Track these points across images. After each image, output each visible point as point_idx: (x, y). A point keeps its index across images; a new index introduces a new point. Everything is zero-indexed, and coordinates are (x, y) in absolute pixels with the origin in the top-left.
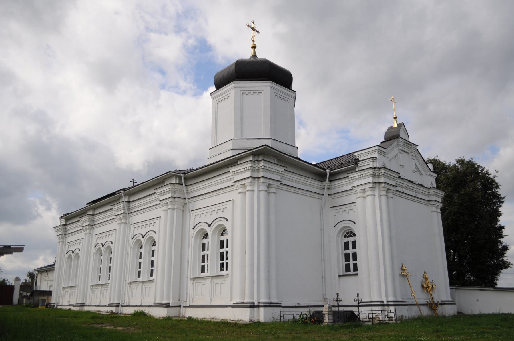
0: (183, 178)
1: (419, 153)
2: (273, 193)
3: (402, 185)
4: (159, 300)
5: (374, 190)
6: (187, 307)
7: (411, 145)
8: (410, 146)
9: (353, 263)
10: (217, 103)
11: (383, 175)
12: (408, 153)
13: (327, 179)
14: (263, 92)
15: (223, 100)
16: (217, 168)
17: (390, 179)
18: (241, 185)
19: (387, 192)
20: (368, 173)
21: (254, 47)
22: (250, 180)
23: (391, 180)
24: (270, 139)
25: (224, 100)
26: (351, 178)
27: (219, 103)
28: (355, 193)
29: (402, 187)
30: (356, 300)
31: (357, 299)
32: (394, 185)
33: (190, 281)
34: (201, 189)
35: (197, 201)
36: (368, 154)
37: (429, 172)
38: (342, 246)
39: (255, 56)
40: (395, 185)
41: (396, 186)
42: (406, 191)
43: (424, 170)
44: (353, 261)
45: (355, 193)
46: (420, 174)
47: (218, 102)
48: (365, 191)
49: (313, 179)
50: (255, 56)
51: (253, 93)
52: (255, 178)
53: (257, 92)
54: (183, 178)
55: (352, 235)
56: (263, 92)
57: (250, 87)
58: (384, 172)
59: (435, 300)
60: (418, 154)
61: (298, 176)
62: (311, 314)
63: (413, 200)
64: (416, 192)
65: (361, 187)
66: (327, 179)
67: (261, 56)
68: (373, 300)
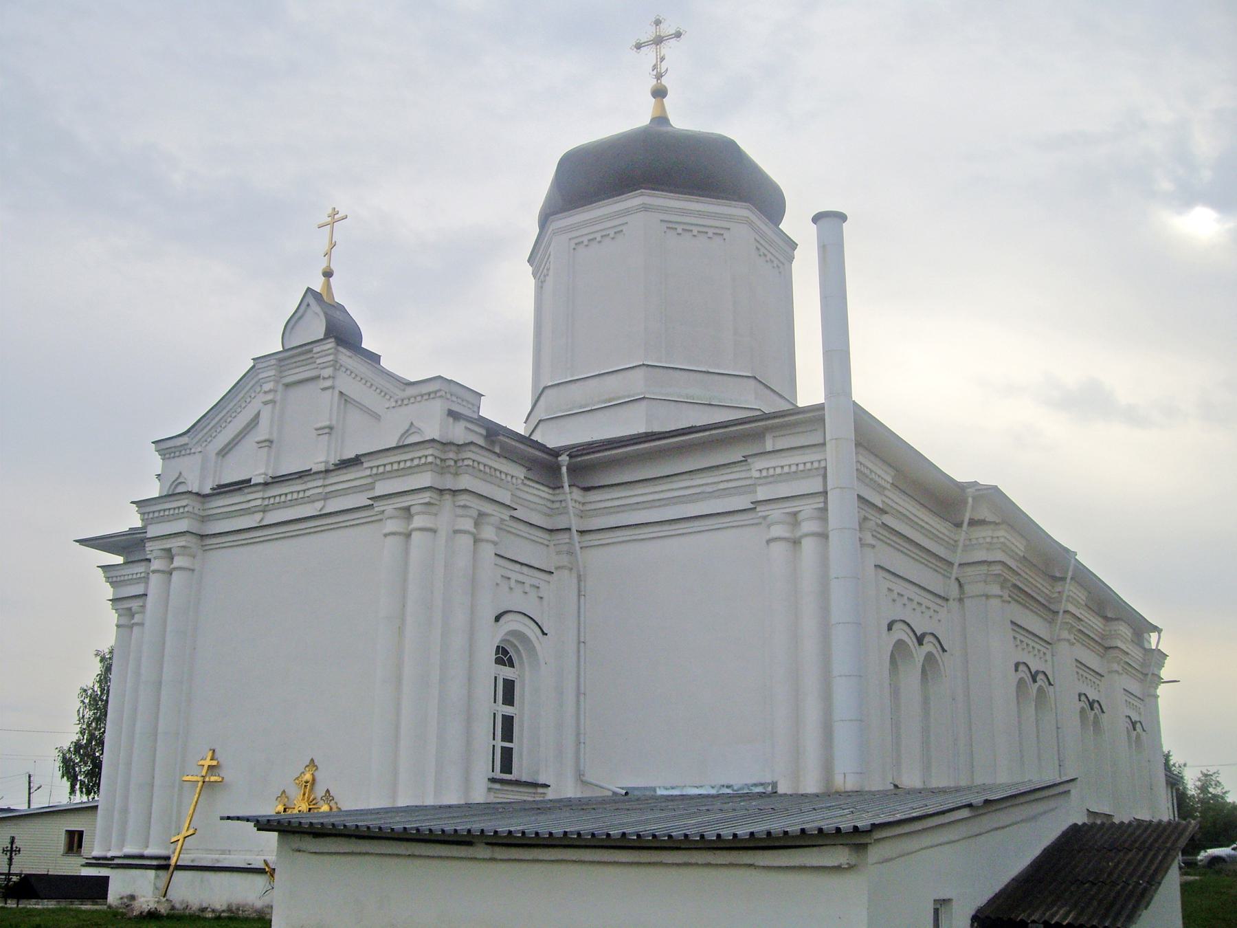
0: (564, 469)
5: (436, 515)
7: (311, 351)
8: (310, 355)
10: (573, 246)
11: (431, 463)
13: (566, 485)
14: (726, 234)
19: (477, 524)
21: (659, 93)
25: (598, 239)
26: (371, 468)
28: (381, 520)
30: (15, 851)
31: (9, 849)
33: (208, 769)
35: (509, 532)
39: (661, 119)
44: (503, 740)
45: (381, 520)
48: (410, 513)
49: (532, 480)
50: (661, 119)
54: (564, 469)
55: (500, 655)
56: (726, 234)
58: (432, 455)
59: (7, 866)
63: (329, 527)
65: (400, 499)
66: (566, 485)
67: (683, 120)
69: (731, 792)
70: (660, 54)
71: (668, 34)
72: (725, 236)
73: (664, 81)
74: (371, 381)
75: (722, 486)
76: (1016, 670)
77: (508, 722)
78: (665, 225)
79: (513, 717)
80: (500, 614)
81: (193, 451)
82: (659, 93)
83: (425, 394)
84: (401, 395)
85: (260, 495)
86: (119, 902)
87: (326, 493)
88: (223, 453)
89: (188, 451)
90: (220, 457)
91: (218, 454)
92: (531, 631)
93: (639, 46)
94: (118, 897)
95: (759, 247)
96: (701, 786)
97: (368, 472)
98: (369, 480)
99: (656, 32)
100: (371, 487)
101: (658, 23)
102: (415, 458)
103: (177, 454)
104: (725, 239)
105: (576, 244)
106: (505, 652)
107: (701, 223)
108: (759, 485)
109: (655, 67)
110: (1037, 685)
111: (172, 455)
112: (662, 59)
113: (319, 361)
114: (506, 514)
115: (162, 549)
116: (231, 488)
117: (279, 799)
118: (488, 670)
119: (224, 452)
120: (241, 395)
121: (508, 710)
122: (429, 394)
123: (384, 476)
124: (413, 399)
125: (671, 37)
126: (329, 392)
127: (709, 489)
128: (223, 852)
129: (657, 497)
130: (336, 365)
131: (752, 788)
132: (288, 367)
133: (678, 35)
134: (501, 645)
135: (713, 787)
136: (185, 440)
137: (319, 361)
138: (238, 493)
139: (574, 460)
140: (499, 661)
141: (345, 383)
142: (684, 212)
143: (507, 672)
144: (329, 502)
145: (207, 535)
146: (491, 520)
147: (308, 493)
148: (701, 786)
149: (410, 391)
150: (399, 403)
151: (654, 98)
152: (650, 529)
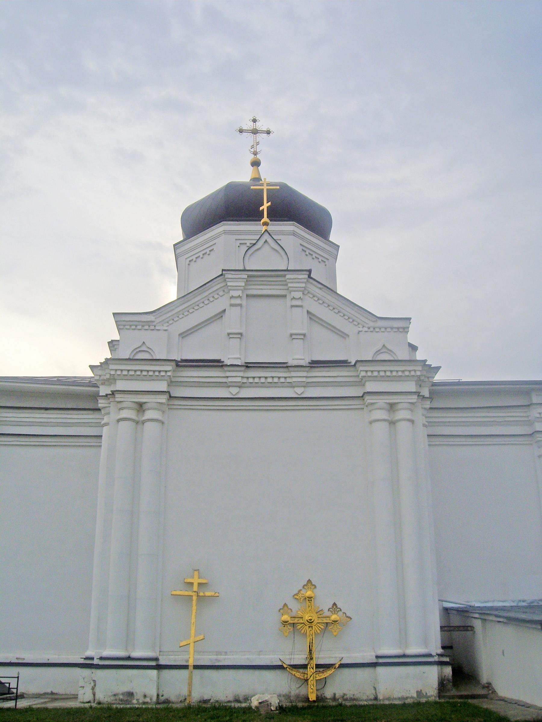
1: (322, 286)
2: (404, 420)
3: (224, 380)
4: (286, 705)
7: (285, 276)
8: (283, 279)
10: (188, 262)
12: (284, 296)
15: (206, 253)
27: (192, 263)
29: (226, 385)
37: (374, 321)
42: (244, 394)
43: (353, 321)
46: (341, 336)
47: (190, 261)
60: (320, 289)
61: (43, 411)
62: (5, 684)
63: (306, 408)
64: (292, 385)
68: (134, 654)
69: (526, 604)
70: (256, 140)
71: (261, 130)
72: (327, 263)
73: (258, 156)
74: (339, 308)
75: (507, 419)
78: (302, 247)
81: (157, 328)
82: (256, 164)
83: (395, 328)
84: (371, 324)
85: (241, 374)
86: (113, 698)
87: (307, 382)
88: (183, 336)
89: (152, 327)
90: (181, 338)
91: (180, 335)
93: (268, 132)
94: (111, 694)
96: (505, 601)
99: (254, 126)
101: (254, 121)
102: (406, 370)
103: (139, 327)
104: (326, 265)
105: (240, 244)
107: (212, 244)
108: (538, 422)
109: (252, 147)
111: (133, 327)
112: (258, 143)
113: (290, 285)
115: (134, 402)
116: (205, 364)
117: (281, 611)
119: (184, 335)
120: (206, 294)
122: (398, 328)
123: (375, 379)
124: (384, 329)
125: (263, 132)
126: (299, 309)
127: (498, 420)
128: (219, 653)
129: (463, 420)
130: (305, 292)
131: (540, 602)
132: (253, 283)
133: (254, 121)
135: (514, 602)
136: (151, 318)
137: (290, 285)
138: (220, 369)
139: (434, 388)
141: (310, 304)
142: (310, 242)
144: (307, 389)
145: (176, 397)
147: (230, 380)
148: (505, 601)
149: (380, 323)
150: (372, 329)
151: (253, 167)
152: (458, 439)
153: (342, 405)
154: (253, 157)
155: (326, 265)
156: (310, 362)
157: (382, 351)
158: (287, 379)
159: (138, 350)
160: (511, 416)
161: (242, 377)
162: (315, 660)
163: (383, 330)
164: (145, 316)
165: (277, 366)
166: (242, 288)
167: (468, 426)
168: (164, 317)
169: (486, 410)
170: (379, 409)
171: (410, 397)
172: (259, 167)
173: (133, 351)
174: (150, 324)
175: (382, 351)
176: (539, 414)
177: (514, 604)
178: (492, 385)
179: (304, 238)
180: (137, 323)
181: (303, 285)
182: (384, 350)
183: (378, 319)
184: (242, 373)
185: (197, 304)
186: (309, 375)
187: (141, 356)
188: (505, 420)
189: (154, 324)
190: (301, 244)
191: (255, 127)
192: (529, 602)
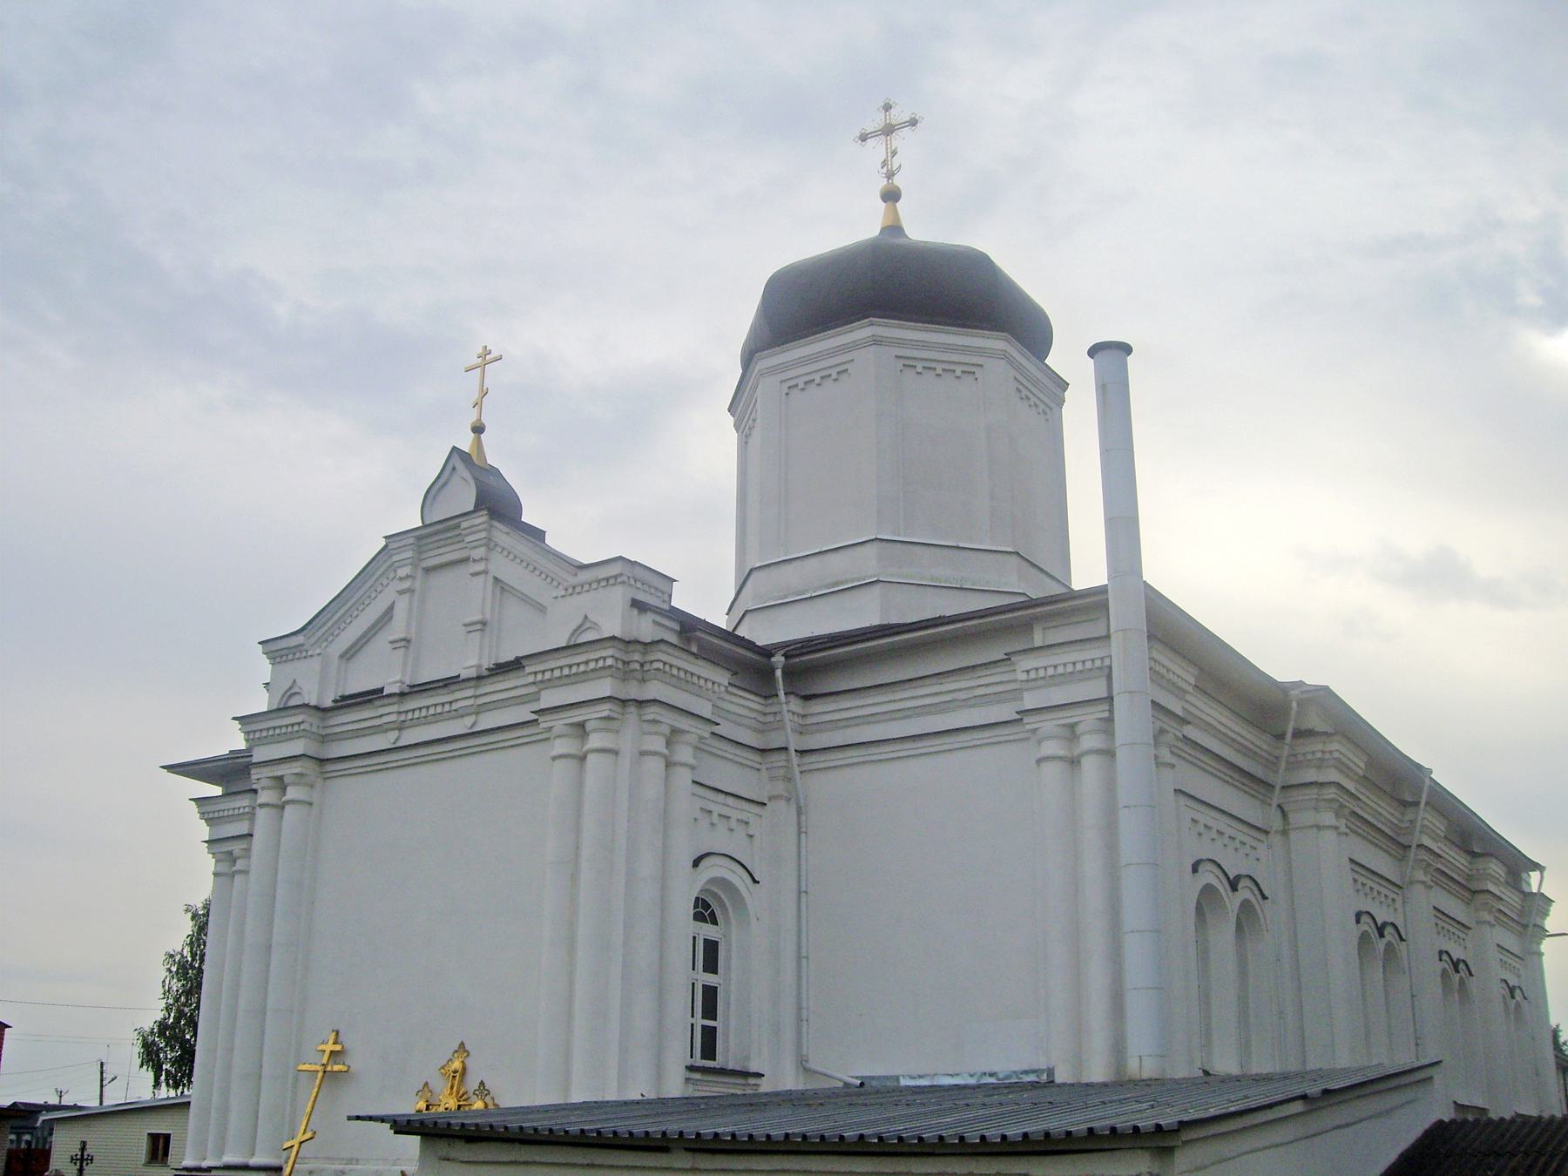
0: (779, 673)
6: (363, 1117)
7: (458, 526)
8: (457, 532)
9: (716, 1020)
16: (972, 635)
17: (279, 742)
18: (568, 727)
20: (1045, 668)
22: (605, 710)
23: (283, 741)
24: (873, 540)
32: (1179, 712)
34: (887, 717)
36: (281, 657)
38: (728, 958)
39: (893, 229)
40: (1181, 714)
41: (1183, 721)
50: (894, 229)
51: (822, 378)
52: (624, 702)
53: (834, 372)
57: (809, 359)
67: (922, 229)
69: (995, 1081)
72: (977, 375)
76: (1358, 921)
77: (710, 994)
79: (716, 987)
80: (699, 858)
84: (573, 581)
85: (394, 708)
89: (304, 654)
92: (738, 878)
95: (1021, 387)
97: (531, 679)
98: (533, 689)
100: (535, 697)
101: (887, 108)
103: (290, 657)
104: (976, 379)
105: (789, 388)
106: (706, 905)
109: (884, 164)
110: (1384, 941)
112: (894, 153)
114: (705, 730)
118: (684, 927)
119: (349, 655)
121: (711, 979)
122: (607, 579)
134: (701, 897)
135: (972, 1076)
136: (300, 639)
140: (698, 917)
142: (926, 345)
143: (708, 931)
146: (688, 737)
149: (584, 576)
150: (570, 591)
151: (885, 202)
153: (524, 736)
154: (886, 183)
155: (1047, 420)
156: (492, 666)
157: (585, 627)
158: (453, 704)
159: (289, 694)
160: (997, 683)
161: (399, 713)
162: (287, 1162)
163: (594, 585)
164: (294, 638)
165: (432, 686)
166: (484, 541)
167: (909, 717)
168: (319, 634)
169: (934, 680)
170: (559, 736)
171: (598, 708)
172: (897, 204)
173: (283, 696)
174: (301, 648)
175: (585, 627)
176: (1025, 673)
177: (972, 1081)
178: (936, 626)
179: (905, 342)
180: (286, 651)
181: (483, 535)
182: (588, 625)
183: (578, 570)
184: (472, 690)
185: (361, 601)
186: (478, 693)
187: (293, 702)
188: (976, 694)
189: (304, 648)
190: (896, 356)
191: (888, 121)
192: (1001, 1076)
